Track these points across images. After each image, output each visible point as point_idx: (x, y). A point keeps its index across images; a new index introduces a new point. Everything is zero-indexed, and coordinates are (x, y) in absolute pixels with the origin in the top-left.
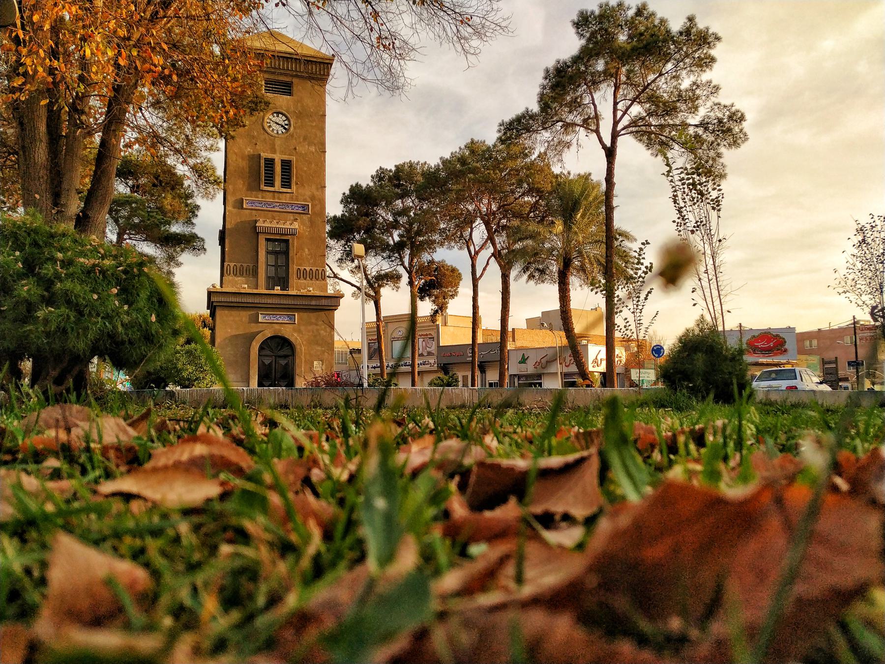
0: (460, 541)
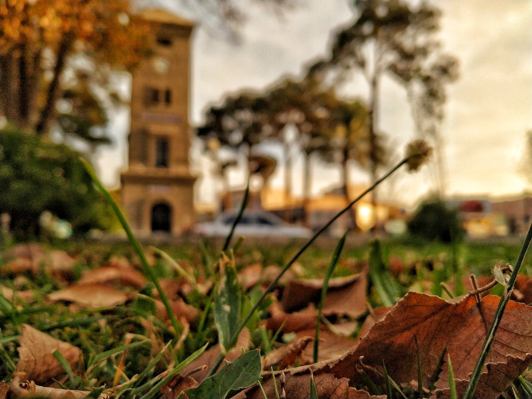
0: (277, 332)
